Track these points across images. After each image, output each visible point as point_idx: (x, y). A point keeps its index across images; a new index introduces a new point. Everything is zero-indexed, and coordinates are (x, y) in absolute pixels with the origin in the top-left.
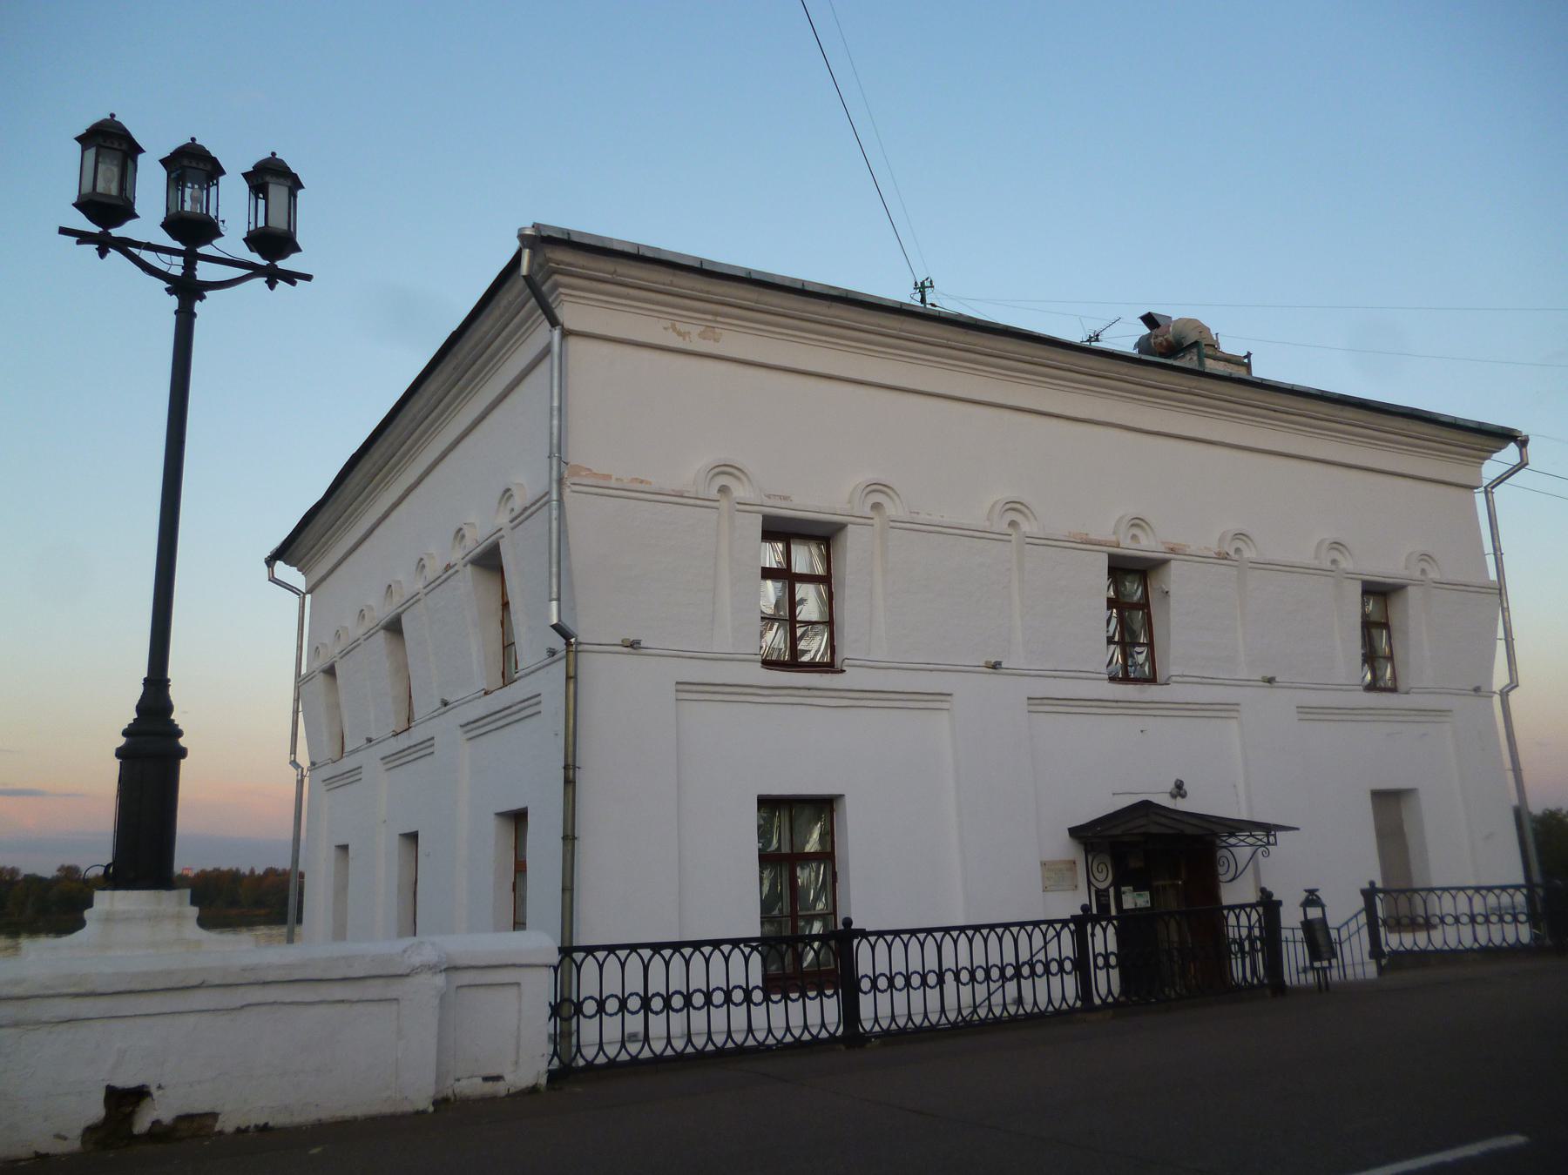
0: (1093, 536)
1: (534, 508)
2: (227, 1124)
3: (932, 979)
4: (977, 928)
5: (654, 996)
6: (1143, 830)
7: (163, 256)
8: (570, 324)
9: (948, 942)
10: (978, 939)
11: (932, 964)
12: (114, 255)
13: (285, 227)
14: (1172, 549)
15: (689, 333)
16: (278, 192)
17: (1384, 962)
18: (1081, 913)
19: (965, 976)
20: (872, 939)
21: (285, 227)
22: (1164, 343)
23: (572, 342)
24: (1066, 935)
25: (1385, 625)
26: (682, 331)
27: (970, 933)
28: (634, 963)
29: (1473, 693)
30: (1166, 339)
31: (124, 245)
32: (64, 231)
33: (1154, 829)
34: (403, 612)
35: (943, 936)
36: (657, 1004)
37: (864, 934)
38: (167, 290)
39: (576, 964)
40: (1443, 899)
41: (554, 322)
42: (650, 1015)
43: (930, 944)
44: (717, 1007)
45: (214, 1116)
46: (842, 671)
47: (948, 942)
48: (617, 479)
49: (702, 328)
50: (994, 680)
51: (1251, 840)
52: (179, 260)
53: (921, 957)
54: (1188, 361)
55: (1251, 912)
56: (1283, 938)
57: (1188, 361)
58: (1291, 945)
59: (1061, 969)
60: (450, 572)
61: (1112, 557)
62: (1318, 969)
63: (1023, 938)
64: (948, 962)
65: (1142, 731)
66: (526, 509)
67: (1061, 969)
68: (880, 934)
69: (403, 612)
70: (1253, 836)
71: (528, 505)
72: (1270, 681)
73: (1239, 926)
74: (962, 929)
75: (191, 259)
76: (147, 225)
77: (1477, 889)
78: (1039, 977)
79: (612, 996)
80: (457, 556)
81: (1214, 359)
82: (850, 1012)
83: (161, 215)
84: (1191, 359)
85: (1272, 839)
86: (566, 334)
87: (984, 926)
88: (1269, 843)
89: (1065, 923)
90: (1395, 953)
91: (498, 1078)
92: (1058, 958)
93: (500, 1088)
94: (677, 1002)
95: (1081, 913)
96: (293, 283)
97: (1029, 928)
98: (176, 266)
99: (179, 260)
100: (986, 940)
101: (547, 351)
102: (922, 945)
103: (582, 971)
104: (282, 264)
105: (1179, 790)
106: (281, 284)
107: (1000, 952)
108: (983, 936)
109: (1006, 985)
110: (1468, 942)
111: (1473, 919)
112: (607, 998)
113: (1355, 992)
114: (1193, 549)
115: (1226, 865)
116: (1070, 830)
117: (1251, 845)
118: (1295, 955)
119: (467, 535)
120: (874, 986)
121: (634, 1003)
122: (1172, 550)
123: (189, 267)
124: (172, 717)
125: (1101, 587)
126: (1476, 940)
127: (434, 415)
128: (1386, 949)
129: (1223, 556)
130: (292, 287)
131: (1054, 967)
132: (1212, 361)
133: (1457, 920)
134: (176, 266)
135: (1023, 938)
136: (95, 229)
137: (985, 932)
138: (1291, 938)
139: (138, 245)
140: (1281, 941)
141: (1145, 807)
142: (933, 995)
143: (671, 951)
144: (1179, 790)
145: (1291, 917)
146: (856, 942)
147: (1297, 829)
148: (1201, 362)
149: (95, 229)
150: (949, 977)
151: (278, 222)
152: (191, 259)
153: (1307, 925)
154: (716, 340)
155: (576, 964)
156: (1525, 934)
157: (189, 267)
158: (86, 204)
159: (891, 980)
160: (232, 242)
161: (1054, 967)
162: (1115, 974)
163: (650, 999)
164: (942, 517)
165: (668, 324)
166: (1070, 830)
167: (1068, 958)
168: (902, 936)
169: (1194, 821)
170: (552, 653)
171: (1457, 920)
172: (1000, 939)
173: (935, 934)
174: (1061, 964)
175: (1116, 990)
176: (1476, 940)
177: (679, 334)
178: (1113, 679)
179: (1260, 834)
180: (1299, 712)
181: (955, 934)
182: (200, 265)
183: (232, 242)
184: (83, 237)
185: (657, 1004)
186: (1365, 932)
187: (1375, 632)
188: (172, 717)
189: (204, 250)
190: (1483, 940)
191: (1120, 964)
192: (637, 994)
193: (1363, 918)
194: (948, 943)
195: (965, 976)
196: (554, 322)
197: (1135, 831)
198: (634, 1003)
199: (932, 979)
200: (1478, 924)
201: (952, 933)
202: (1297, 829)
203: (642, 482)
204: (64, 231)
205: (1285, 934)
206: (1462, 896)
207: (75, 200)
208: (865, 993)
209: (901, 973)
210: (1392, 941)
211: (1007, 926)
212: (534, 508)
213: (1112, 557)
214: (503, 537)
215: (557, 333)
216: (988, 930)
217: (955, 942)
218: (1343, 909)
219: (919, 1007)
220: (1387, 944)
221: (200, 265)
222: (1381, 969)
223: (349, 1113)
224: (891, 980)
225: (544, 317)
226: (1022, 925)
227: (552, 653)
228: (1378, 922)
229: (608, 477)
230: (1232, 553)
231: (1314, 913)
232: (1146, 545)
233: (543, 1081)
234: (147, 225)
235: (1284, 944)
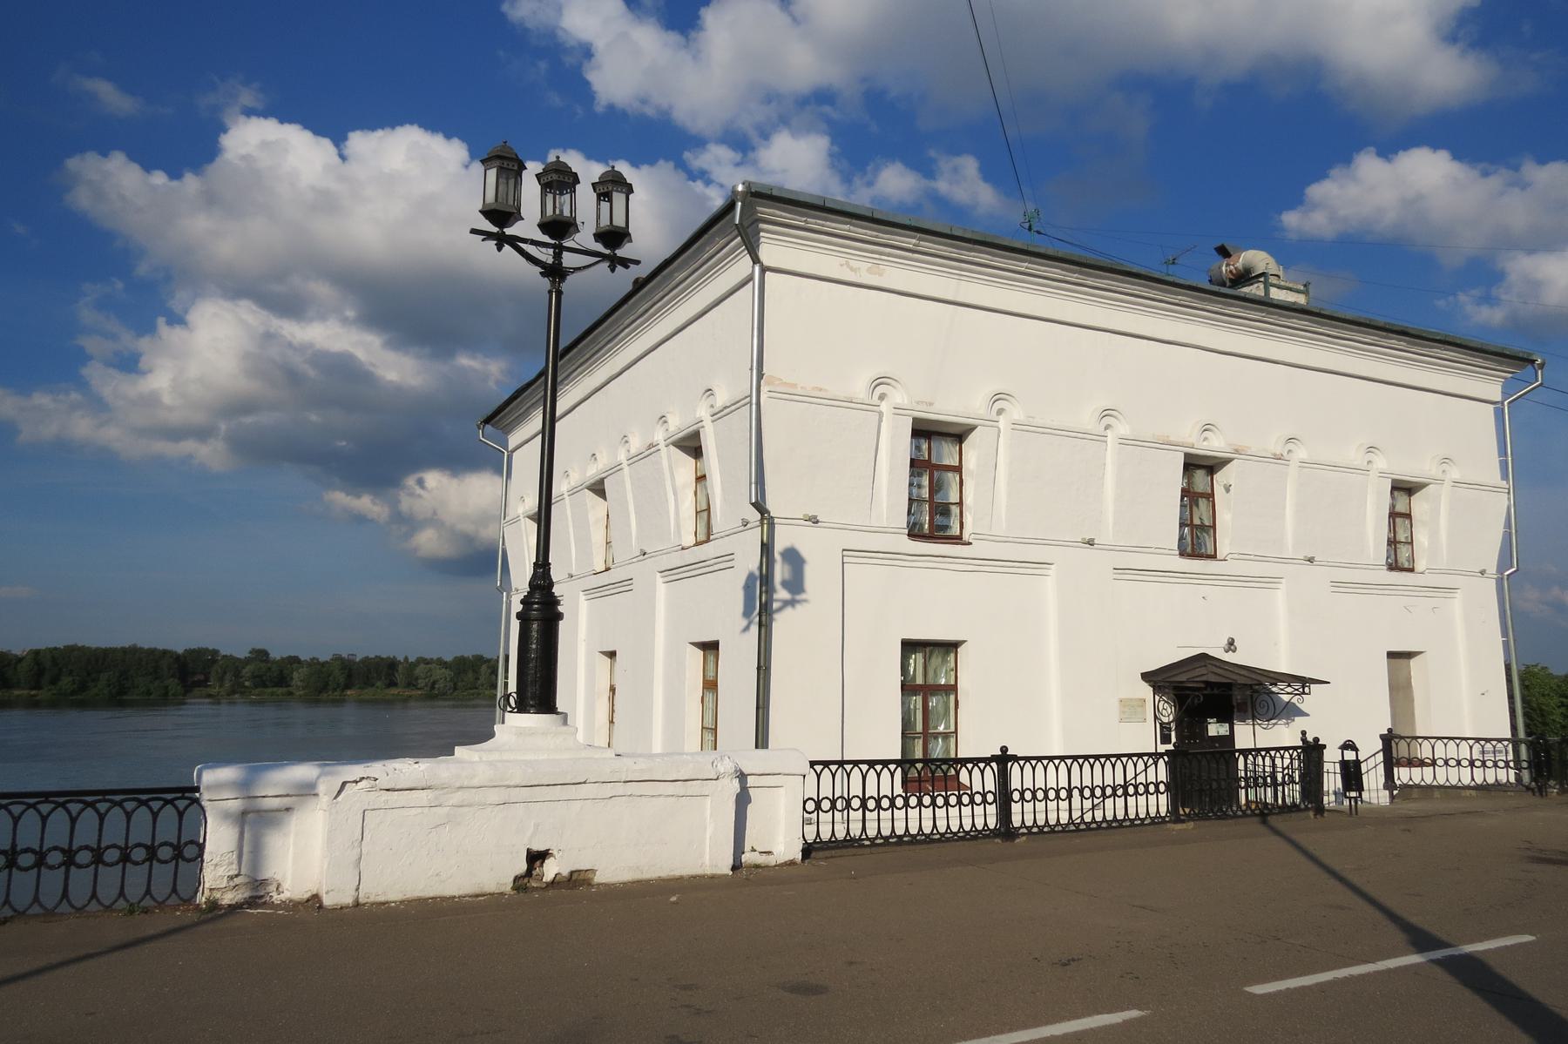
0: (1173, 439)
1: (733, 408)
2: (599, 878)
3: (1063, 794)
4: (1075, 758)
5: (869, 798)
6: (1204, 678)
7: (544, 250)
8: (766, 261)
9: (1076, 767)
10: (1097, 766)
11: (1063, 783)
12: (507, 248)
13: (623, 225)
14: (1236, 450)
15: (859, 269)
16: (618, 198)
17: (1395, 792)
18: (1000, 753)
19: (1087, 793)
20: (1022, 762)
21: (623, 225)
22: (1234, 271)
23: (768, 274)
24: (1161, 763)
25: (1408, 516)
26: (855, 267)
27: (1092, 760)
28: (856, 775)
29: (1480, 575)
30: (1236, 268)
31: (514, 241)
32: (474, 231)
33: (1213, 679)
34: (605, 478)
35: (1073, 762)
36: (871, 804)
37: (1015, 758)
38: (541, 273)
39: (846, 771)
40: (134, 817)
41: (756, 260)
42: (936, 808)
43: (1063, 768)
44: (912, 808)
45: (593, 871)
46: (970, 544)
47: (1076, 767)
48: (802, 388)
49: (870, 265)
50: (1088, 551)
51: (1289, 690)
52: (551, 251)
53: (1055, 777)
54: (1256, 290)
55: (1094, 763)
56: (1325, 770)
57: (1256, 290)
58: (1331, 775)
59: (1157, 791)
60: (652, 450)
61: (1187, 455)
62: (1350, 798)
63: (1130, 766)
64: (1075, 782)
66: (726, 408)
67: (1157, 791)
68: (1028, 759)
69: (605, 478)
70: (1290, 686)
71: (728, 405)
72: (1311, 560)
73: (1264, 766)
74: (1062, 758)
75: (559, 250)
76: (527, 227)
77: (1477, 740)
78: (1141, 795)
79: (826, 812)
80: (659, 436)
81: (1278, 288)
82: (1005, 813)
83: (537, 218)
84: (1258, 287)
85: (1307, 690)
86: (764, 270)
87: (1102, 756)
88: (1304, 693)
89: (987, 761)
90: (1405, 787)
91: (769, 853)
92: (1154, 781)
93: (771, 860)
94: (885, 803)
95: (1000, 753)
96: (627, 267)
97: (1135, 759)
98: (546, 256)
99: (551, 251)
100: (1103, 767)
101: (750, 279)
102: (1034, 769)
103: (184, 818)
104: (620, 253)
105: (1231, 645)
106: (619, 268)
107: (1112, 775)
108: (1055, 765)
109: (1106, 801)
110: (1466, 780)
111: (1472, 764)
112: (143, 862)
113: (1378, 818)
114: (1253, 451)
115: (1266, 708)
116: (1142, 674)
117: (1288, 693)
118: (1332, 781)
119: (670, 421)
120: (1022, 798)
121: (856, 803)
122: (1237, 451)
123: (557, 256)
124: (553, 591)
125: (1176, 480)
126: (1473, 779)
127: (638, 322)
128: (1398, 783)
129: (1279, 458)
130: (1225, 245)
131: (1152, 788)
132: (1276, 289)
133: (1459, 763)
134: (546, 256)
135: (1130, 766)
136: (495, 229)
137: (1103, 760)
138: (1331, 770)
139: (525, 241)
140: (1323, 772)
141: (1203, 657)
142: (1064, 805)
143: (895, 766)
144: (1231, 645)
145: (1332, 756)
146: (1010, 764)
147: (1329, 683)
148: (1267, 292)
149: (495, 229)
150: (1076, 793)
151: (619, 221)
152: (559, 250)
153: (1344, 764)
154: (881, 275)
155: (846, 771)
156: (1506, 776)
157: (557, 256)
158: (488, 213)
159: (1034, 793)
160: (585, 237)
161: (1152, 788)
162: (1163, 799)
163: (1067, 797)
164: (1053, 421)
165: (843, 261)
166: (1142, 674)
167: (1162, 782)
168: (860, 766)
169: (1243, 672)
170: (745, 523)
171: (1459, 763)
172: (1114, 766)
173: (831, 767)
174: (1157, 785)
175: (1163, 811)
176: (1473, 779)
177: (852, 269)
178: (1182, 554)
179: (1297, 685)
180: (586, 595)
181: (1057, 762)
182: (565, 254)
183: (585, 237)
184: (488, 235)
185: (871, 804)
186: (1381, 768)
187: (1398, 520)
188: (553, 591)
189: (568, 243)
190: (1479, 780)
191: (1167, 790)
192: (858, 797)
193: (1380, 757)
194: (872, 775)
195: (1087, 793)
196: (756, 260)
197: (1198, 679)
198: (856, 803)
199: (1063, 794)
200: (1476, 767)
201: (1020, 762)
202: (1329, 683)
203: (821, 390)
204: (474, 231)
205: (1326, 767)
206: (1464, 745)
207: (480, 207)
208: (1016, 802)
209: (1041, 789)
210: (1403, 775)
211: (1118, 757)
212: (733, 408)
213: (1187, 455)
214: (703, 427)
215: (757, 268)
216: (852, 766)
217: (1081, 767)
218: (1370, 748)
219: (1058, 813)
220: (1399, 778)
221: (565, 254)
222: (1392, 797)
223: (677, 873)
224: (1034, 793)
225: (746, 252)
226: (1130, 756)
227: (745, 523)
228: (1392, 761)
229: (794, 386)
230: (1285, 454)
231: (1350, 755)
232: (1213, 445)
233: (799, 856)
234: (527, 227)
235: (1325, 775)
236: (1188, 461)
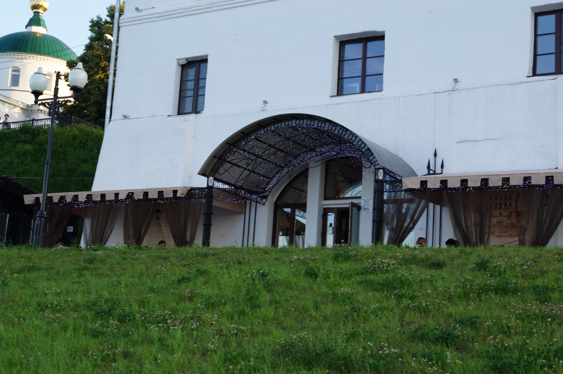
65: (125, 117)
236: (323, 199)
